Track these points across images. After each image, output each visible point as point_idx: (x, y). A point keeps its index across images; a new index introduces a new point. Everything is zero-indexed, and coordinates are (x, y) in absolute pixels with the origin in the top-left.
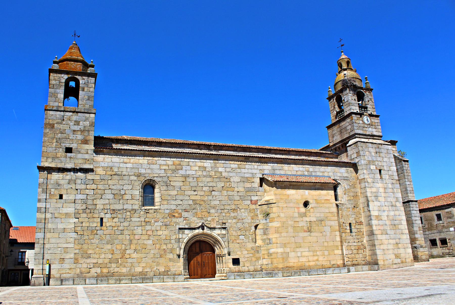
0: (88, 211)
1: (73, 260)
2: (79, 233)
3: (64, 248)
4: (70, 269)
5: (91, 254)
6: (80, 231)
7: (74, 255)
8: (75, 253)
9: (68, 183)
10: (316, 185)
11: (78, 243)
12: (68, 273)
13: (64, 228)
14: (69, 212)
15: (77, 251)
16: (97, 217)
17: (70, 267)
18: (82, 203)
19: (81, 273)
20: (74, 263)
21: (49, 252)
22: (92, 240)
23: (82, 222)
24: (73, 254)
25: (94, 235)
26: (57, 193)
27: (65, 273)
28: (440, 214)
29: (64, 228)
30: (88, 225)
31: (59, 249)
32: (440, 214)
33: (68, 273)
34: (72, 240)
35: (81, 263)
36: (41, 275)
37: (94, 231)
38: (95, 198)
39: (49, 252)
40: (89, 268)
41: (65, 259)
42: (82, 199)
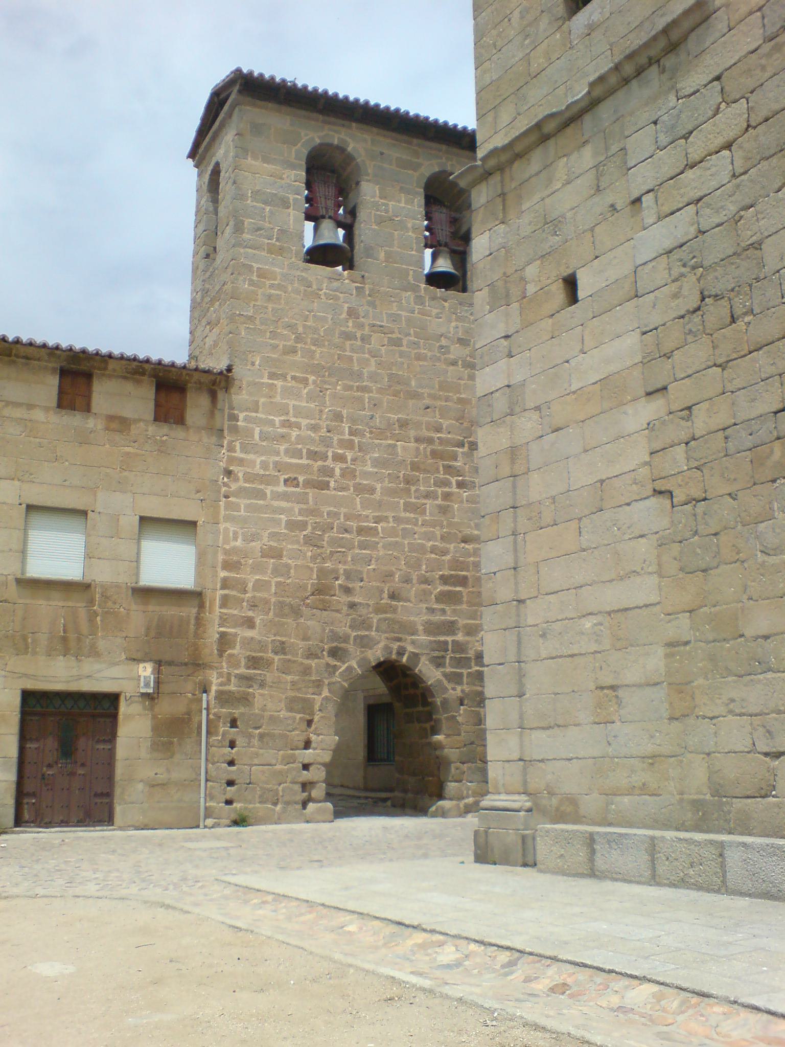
0: (716, 312)
1: (660, 693)
2: (679, 496)
3: (609, 613)
4: (652, 760)
5: (766, 637)
6: (680, 478)
7: (667, 656)
8: (670, 644)
9: (592, 192)
10: (715, 120)
11: (681, 569)
12: (644, 789)
13: (602, 481)
14: (613, 368)
15: (682, 627)
16: (770, 339)
17: (650, 748)
18: (677, 270)
19: (716, 793)
20: (672, 718)
21: (546, 648)
22: (762, 526)
23: (689, 408)
24: (661, 651)
25: (774, 481)
26: (553, 275)
27: (631, 791)
28: (27, 696)
29: (599, 478)
30: (722, 418)
31: (588, 624)
32: (27, 696)
33: (644, 789)
34: (644, 547)
35: (712, 718)
36: (516, 797)
37: (772, 452)
38: (748, 201)
39: (546, 648)
40: (766, 754)
41: (620, 693)
42: (670, 252)
